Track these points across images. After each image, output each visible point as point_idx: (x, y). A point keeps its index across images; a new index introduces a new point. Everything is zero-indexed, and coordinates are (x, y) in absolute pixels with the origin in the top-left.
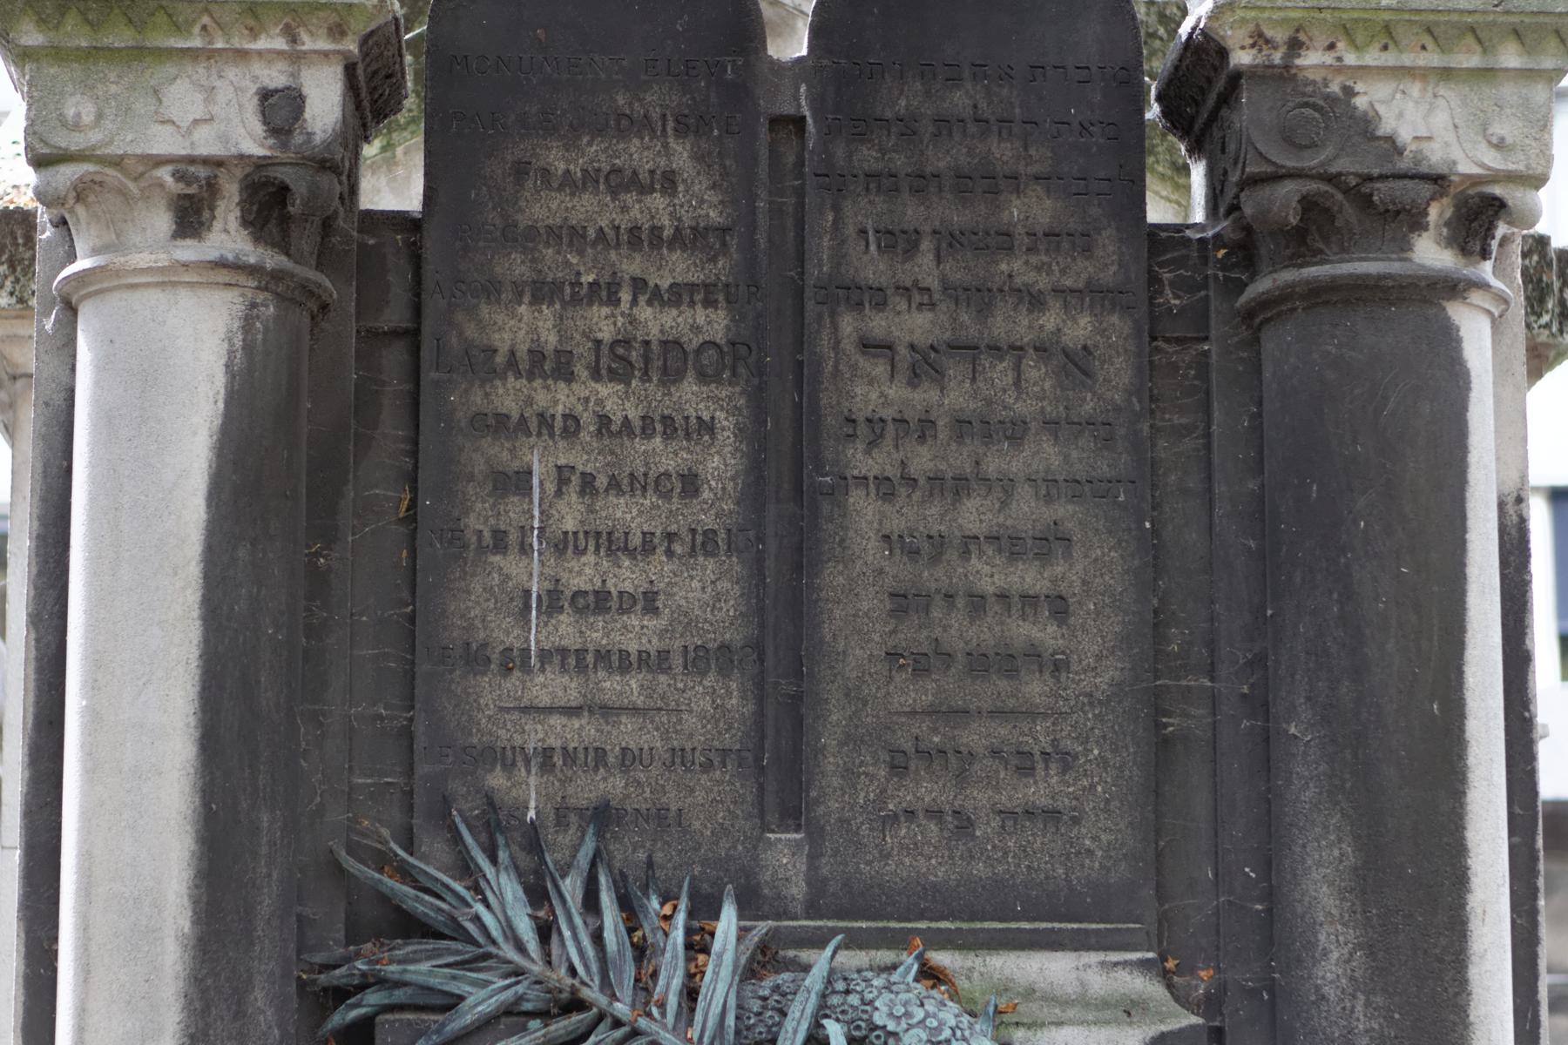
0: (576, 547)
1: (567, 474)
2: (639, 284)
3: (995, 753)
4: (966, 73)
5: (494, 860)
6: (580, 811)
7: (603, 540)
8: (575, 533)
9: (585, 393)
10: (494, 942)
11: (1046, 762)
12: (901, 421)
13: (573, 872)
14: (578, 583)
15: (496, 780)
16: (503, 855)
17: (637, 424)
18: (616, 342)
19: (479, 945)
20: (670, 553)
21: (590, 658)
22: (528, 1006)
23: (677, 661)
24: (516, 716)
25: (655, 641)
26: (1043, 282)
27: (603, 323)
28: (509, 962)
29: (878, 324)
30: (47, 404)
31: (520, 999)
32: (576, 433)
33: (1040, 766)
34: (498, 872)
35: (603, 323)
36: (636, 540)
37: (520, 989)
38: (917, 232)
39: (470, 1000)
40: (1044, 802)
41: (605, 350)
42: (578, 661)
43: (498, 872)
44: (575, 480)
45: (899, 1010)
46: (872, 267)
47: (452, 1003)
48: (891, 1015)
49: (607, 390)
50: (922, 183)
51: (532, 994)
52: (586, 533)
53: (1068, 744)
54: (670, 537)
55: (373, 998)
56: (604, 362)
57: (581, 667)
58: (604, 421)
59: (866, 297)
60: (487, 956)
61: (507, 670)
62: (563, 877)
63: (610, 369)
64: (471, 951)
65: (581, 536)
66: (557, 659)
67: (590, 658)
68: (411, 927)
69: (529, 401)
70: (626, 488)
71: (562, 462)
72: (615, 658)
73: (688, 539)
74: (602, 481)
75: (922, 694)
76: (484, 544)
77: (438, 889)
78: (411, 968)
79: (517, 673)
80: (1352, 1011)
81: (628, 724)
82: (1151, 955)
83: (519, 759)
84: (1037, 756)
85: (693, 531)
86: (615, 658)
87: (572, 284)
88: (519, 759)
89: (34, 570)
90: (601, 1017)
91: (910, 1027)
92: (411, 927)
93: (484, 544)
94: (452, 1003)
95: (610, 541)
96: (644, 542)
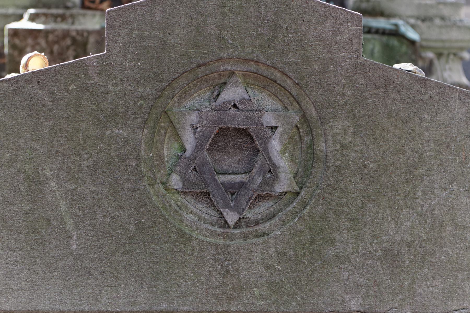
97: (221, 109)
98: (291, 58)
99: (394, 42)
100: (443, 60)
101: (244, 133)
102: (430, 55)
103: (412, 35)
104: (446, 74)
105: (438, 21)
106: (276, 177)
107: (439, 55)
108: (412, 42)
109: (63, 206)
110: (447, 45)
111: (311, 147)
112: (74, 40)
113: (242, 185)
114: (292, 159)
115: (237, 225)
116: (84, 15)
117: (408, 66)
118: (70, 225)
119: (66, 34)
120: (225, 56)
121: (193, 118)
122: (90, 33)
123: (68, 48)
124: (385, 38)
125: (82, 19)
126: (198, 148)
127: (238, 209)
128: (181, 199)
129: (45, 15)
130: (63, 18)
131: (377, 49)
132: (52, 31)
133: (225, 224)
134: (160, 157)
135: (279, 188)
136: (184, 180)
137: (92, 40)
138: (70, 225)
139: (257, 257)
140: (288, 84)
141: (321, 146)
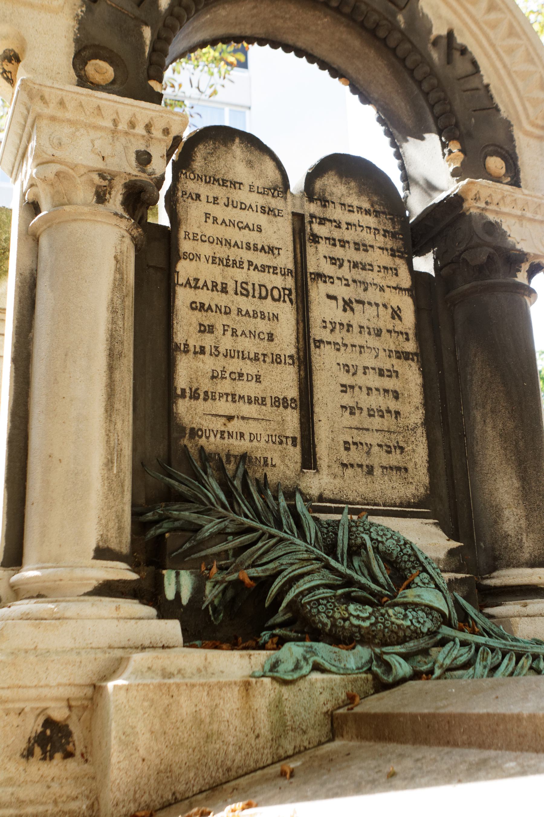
0: (230, 355)
1: (226, 328)
2: (250, 263)
3: (380, 446)
4: (355, 210)
5: (206, 473)
6: (235, 457)
7: (241, 354)
8: (230, 350)
9: (233, 299)
10: (212, 504)
11: (395, 449)
12: (341, 324)
13: (236, 479)
14: (231, 369)
15: (203, 441)
16: (209, 471)
17: (251, 313)
18: (243, 282)
19: (205, 505)
20: (264, 361)
21: (237, 398)
22: (229, 530)
23: (268, 401)
24: (210, 416)
25: (260, 393)
26: (383, 283)
27: (240, 275)
28: (220, 512)
29: (333, 289)
30: (21, 274)
31: (226, 527)
32: (230, 313)
33: (393, 450)
34: (208, 477)
35: (240, 275)
36: (252, 356)
37: (226, 523)
38: (343, 260)
39: (206, 527)
40: (396, 464)
41: (239, 285)
42: (233, 398)
43: (208, 477)
44: (230, 330)
45: (381, 533)
46: (328, 269)
47: (198, 528)
48: (378, 535)
49: (240, 298)
50: (343, 243)
51: (230, 526)
52: (234, 351)
53: (402, 444)
54: (264, 355)
55: (166, 525)
56: (239, 289)
57: (234, 401)
58: (239, 311)
59: (327, 279)
60: (210, 510)
61: (205, 400)
62: (234, 480)
63: (241, 292)
64: (202, 508)
65: (232, 352)
66: (225, 396)
67: (237, 398)
68: (181, 498)
69: (212, 299)
70: (248, 336)
71: (225, 323)
72: (246, 398)
73: (271, 356)
74: (239, 333)
75: (355, 421)
76: (197, 350)
77: (187, 482)
78: (182, 513)
79: (210, 400)
80: (521, 540)
81: (252, 423)
82: (436, 521)
83: (212, 434)
84: (392, 448)
85: (272, 354)
86: (246, 398)
87: (227, 260)
88: (212, 434)
89: (15, 341)
90: (263, 534)
91: (387, 539)
92: (181, 498)
93: (197, 350)
94: (198, 528)
95: (243, 355)
96: (255, 356)
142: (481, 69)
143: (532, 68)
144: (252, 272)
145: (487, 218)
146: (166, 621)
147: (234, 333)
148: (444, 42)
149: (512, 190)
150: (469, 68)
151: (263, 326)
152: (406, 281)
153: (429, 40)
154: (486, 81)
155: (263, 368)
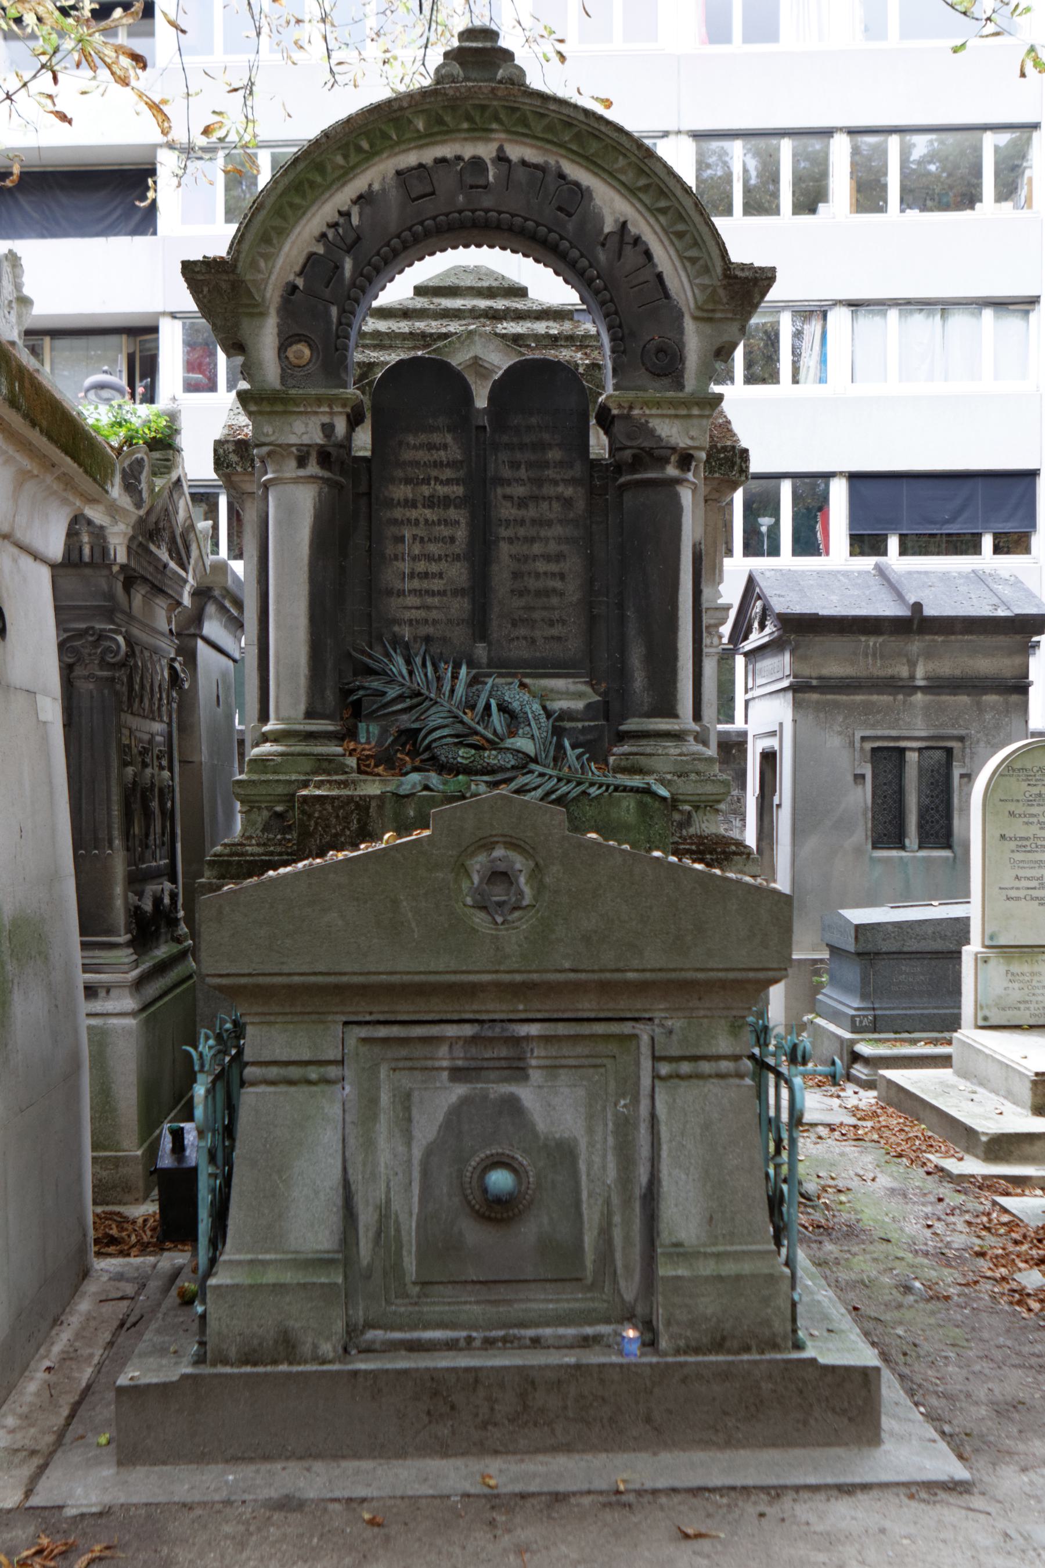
2: (436, 479)
27: (426, 490)
29: (508, 491)
47: (384, 694)
68: (371, 672)
81: (435, 612)
92: (371, 672)
97: (493, 861)
98: (529, 834)
99: (648, 799)
100: (700, 812)
101: (505, 874)
102: (687, 808)
103: (663, 792)
104: (703, 826)
105: (693, 777)
106: (523, 898)
107: (697, 808)
108: (664, 799)
109: (410, 915)
110: (703, 798)
111: (541, 881)
112: (357, 805)
113: (504, 902)
114: (532, 888)
115: (503, 923)
116: (365, 781)
117: (593, 835)
118: (413, 925)
119: (350, 799)
120: (536, 707)
121: (478, 867)
122: (371, 797)
123: (352, 812)
124: (638, 796)
125: (363, 786)
126: (481, 882)
127: (502, 915)
128: (472, 910)
129: (328, 781)
130: (345, 784)
131: (632, 805)
132: (338, 797)
133: (496, 923)
134: (460, 888)
135: (525, 903)
136: (474, 900)
137: (373, 804)
138: (413, 925)
139: (514, 940)
140: (527, 847)
141: (547, 880)
142: (655, 256)
143: (701, 262)
144: (439, 487)
145: (651, 433)
146: (306, 568)
147: (422, 539)
148: (616, 239)
149: (542, 1469)
150: (642, 260)
151: (446, 532)
152: (578, 470)
153: (596, 402)
154: (660, 269)
155: (443, 565)
